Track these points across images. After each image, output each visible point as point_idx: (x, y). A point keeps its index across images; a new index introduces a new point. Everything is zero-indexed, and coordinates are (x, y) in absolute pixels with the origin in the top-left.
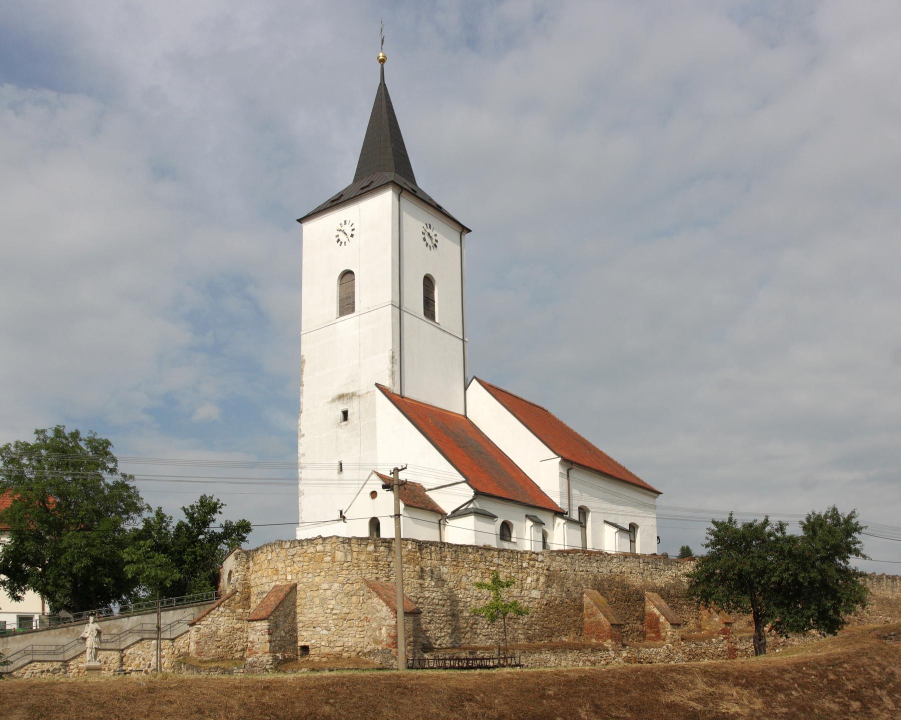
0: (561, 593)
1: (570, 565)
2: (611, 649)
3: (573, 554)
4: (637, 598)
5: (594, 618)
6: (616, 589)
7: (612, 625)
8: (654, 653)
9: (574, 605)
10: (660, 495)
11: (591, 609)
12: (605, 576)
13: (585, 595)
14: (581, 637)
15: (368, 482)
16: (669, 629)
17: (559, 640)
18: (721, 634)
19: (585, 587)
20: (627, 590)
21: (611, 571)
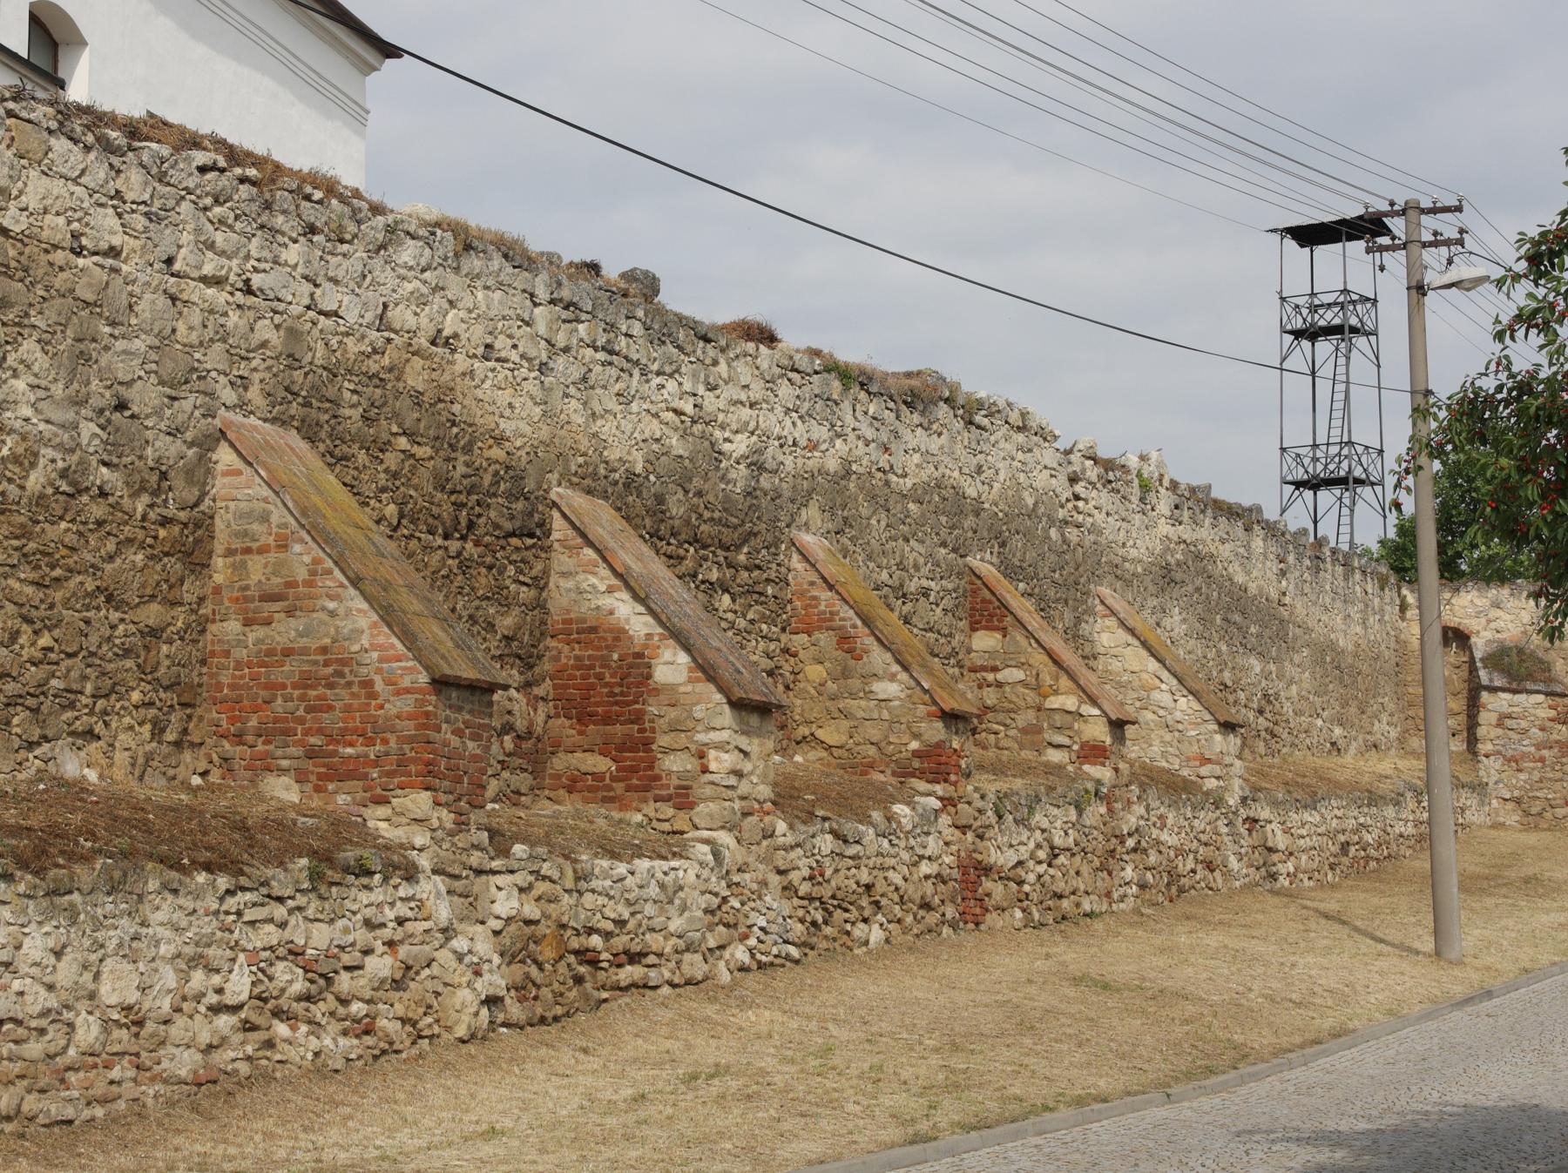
0: (70, 415)
1: (139, 222)
2: (424, 862)
3: (165, 151)
4: (512, 518)
5: (297, 624)
6: (403, 442)
7: (441, 684)
8: (653, 891)
9: (152, 515)
10: (390, 63)
11: (272, 557)
12: (349, 341)
13: (224, 456)
14: (187, 756)
16: (724, 735)
17: (41, 775)
18: (921, 774)
19: (229, 396)
20: (462, 458)
21: (382, 323)
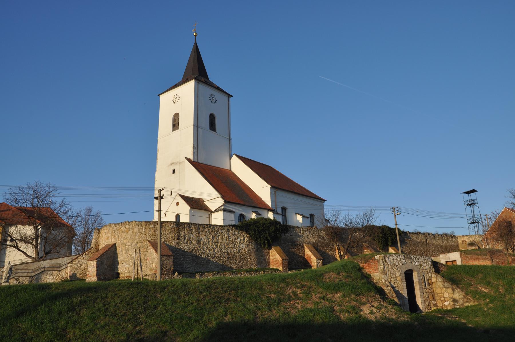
6: (288, 243)
10: (326, 201)
15: (174, 197)
